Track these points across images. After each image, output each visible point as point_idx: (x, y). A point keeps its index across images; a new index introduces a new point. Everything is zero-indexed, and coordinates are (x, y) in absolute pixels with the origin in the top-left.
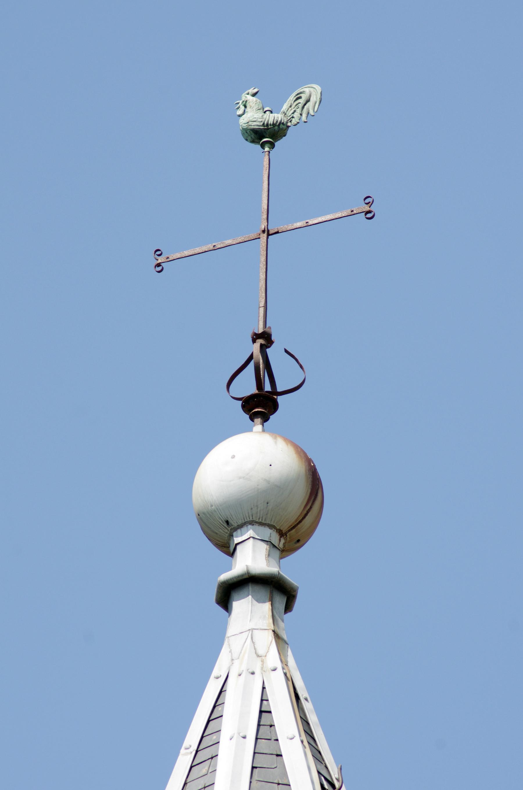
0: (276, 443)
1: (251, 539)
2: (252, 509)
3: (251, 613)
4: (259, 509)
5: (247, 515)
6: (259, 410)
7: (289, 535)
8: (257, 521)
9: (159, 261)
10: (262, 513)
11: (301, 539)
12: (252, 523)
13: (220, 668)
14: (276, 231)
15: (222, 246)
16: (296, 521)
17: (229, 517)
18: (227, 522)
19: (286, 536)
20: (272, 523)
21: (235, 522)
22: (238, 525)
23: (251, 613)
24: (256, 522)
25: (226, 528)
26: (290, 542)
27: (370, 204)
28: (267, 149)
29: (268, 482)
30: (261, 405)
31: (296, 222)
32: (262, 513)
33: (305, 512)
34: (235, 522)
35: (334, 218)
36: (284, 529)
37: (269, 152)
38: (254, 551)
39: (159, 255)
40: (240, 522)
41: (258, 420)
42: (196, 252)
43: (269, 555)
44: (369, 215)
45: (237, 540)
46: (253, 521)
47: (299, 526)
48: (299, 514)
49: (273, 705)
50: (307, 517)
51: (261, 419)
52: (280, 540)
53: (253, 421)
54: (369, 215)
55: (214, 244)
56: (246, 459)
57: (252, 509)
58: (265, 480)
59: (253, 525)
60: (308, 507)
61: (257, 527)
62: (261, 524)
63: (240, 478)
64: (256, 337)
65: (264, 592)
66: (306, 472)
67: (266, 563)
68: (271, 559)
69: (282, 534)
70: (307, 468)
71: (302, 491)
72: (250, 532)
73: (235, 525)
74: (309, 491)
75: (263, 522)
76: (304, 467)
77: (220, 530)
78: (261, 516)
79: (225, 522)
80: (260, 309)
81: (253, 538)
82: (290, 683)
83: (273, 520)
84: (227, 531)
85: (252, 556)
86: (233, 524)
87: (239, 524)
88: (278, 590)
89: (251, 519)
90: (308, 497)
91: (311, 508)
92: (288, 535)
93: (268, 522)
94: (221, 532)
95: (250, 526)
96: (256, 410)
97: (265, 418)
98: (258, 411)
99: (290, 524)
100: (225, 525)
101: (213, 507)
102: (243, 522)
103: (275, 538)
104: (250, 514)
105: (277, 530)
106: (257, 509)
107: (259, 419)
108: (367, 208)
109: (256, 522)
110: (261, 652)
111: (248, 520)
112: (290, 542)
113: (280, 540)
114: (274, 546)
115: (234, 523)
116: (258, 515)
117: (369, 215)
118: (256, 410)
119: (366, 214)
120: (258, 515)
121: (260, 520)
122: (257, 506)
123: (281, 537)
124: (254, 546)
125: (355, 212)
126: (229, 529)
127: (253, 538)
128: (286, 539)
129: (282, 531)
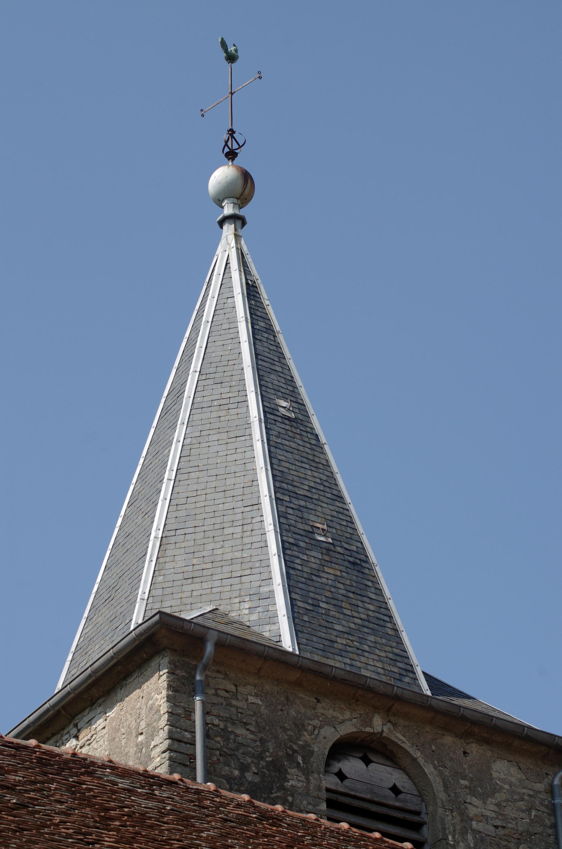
3: (229, 230)
12: (226, 198)
13: (217, 253)
23: (229, 230)
30: (231, 155)
36: (238, 196)
38: (228, 207)
44: (260, 78)
49: (230, 261)
56: (222, 175)
62: (229, 197)
64: (229, 131)
65: (232, 221)
69: (238, 199)
71: (240, 183)
72: (226, 201)
82: (240, 251)
85: (228, 209)
88: (238, 220)
97: (233, 159)
103: (235, 201)
108: (259, 75)
110: (229, 243)
115: (221, 199)
117: (260, 78)
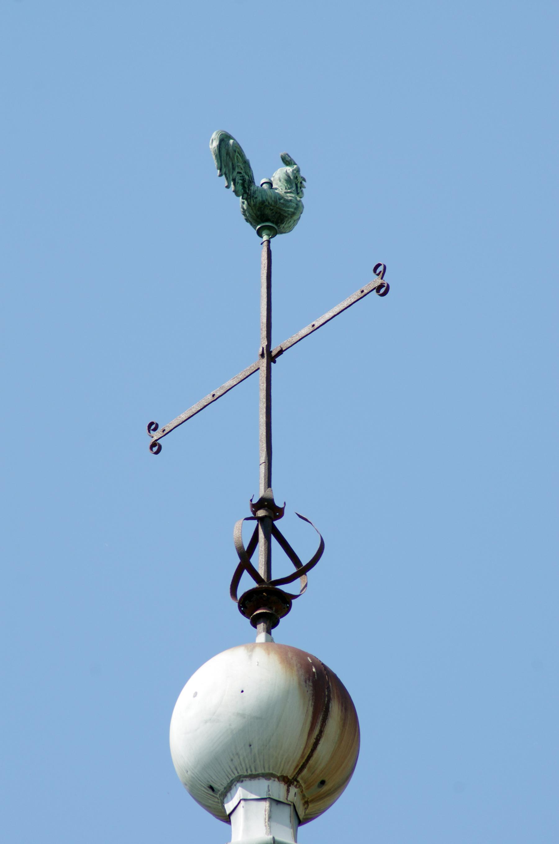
0: (250, 657)
1: (242, 802)
2: (232, 760)
4: (241, 758)
5: (229, 770)
6: (264, 611)
7: (302, 779)
8: (245, 774)
9: (155, 438)
10: (247, 762)
11: (326, 779)
12: (240, 779)
14: (279, 349)
15: (223, 391)
16: (302, 757)
17: (209, 780)
18: (211, 788)
19: (298, 782)
20: (267, 771)
21: (219, 784)
22: (225, 788)
24: (246, 777)
25: (213, 796)
26: (308, 787)
27: (381, 274)
28: (265, 238)
29: (242, 716)
30: (265, 604)
31: (300, 329)
32: (247, 762)
33: (313, 740)
34: (219, 784)
35: (342, 308)
36: (290, 773)
37: (269, 242)
39: (155, 430)
40: (225, 783)
41: (261, 626)
42: (194, 411)
43: (270, 818)
44: (382, 290)
45: (228, 810)
46: (240, 777)
47: (311, 762)
48: (302, 747)
50: (319, 747)
51: (264, 622)
52: (288, 791)
53: (256, 628)
54: (382, 291)
55: (212, 393)
57: (232, 760)
58: (238, 714)
59: (242, 781)
60: (316, 732)
61: (248, 783)
62: (253, 777)
63: (206, 722)
66: (300, 684)
67: (264, 831)
68: (274, 824)
69: (288, 781)
70: (303, 678)
71: (298, 714)
72: (239, 792)
73: (222, 789)
74: (311, 709)
75: (254, 773)
76: (296, 678)
77: (210, 801)
78: (248, 766)
79: (208, 788)
80: (261, 466)
81: (245, 800)
83: (266, 766)
84: (216, 800)
86: (219, 788)
87: (225, 785)
89: (237, 775)
90: (310, 719)
91: (321, 732)
92: (299, 779)
93: (260, 771)
94: (212, 804)
95: (238, 784)
96: (255, 614)
98: (260, 613)
99: (295, 764)
100: (211, 792)
101: (189, 773)
102: (229, 781)
103: (278, 790)
104: (232, 767)
105: (278, 778)
106: (239, 757)
107: (262, 624)
108: (378, 281)
109: (246, 777)
111: (234, 776)
112: (308, 787)
113: (288, 791)
114: (278, 802)
115: (220, 786)
116: (244, 765)
117: (382, 290)
118: (255, 614)
119: (378, 291)
120: (244, 765)
121: (249, 772)
122: (237, 754)
123: (289, 786)
124: (246, 812)
125: (366, 292)
126: (218, 796)
127: (245, 800)
128: (299, 786)
129: (287, 777)
